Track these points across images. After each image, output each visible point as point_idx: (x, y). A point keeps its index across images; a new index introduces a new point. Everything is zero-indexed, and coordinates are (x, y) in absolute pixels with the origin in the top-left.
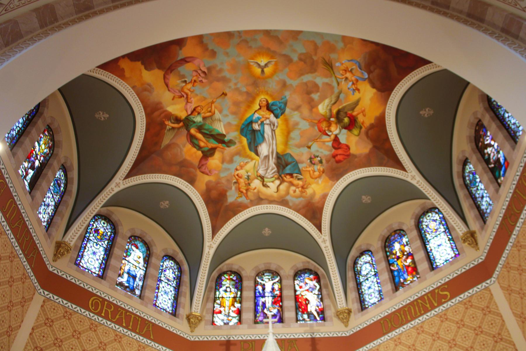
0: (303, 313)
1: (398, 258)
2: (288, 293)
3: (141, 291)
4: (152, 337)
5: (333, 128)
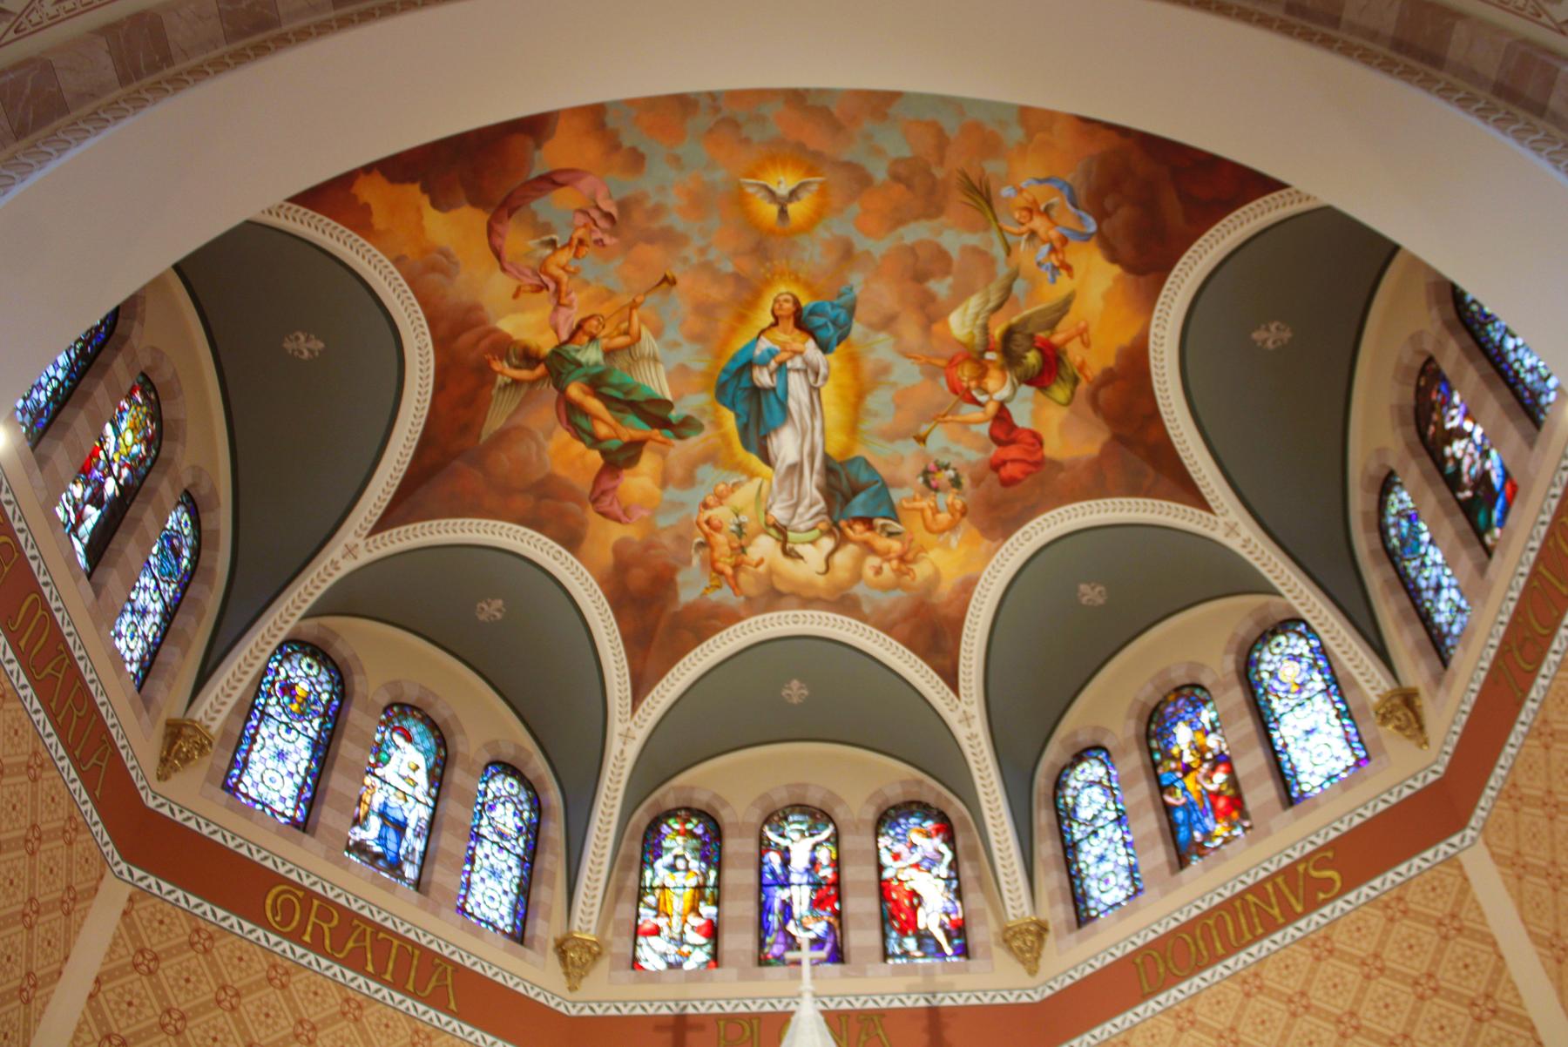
0: (903, 932)
1: (1187, 769)
2: (858, 874)
3: (421, 869)
4: (453, 1006)
5: (992, 382)
